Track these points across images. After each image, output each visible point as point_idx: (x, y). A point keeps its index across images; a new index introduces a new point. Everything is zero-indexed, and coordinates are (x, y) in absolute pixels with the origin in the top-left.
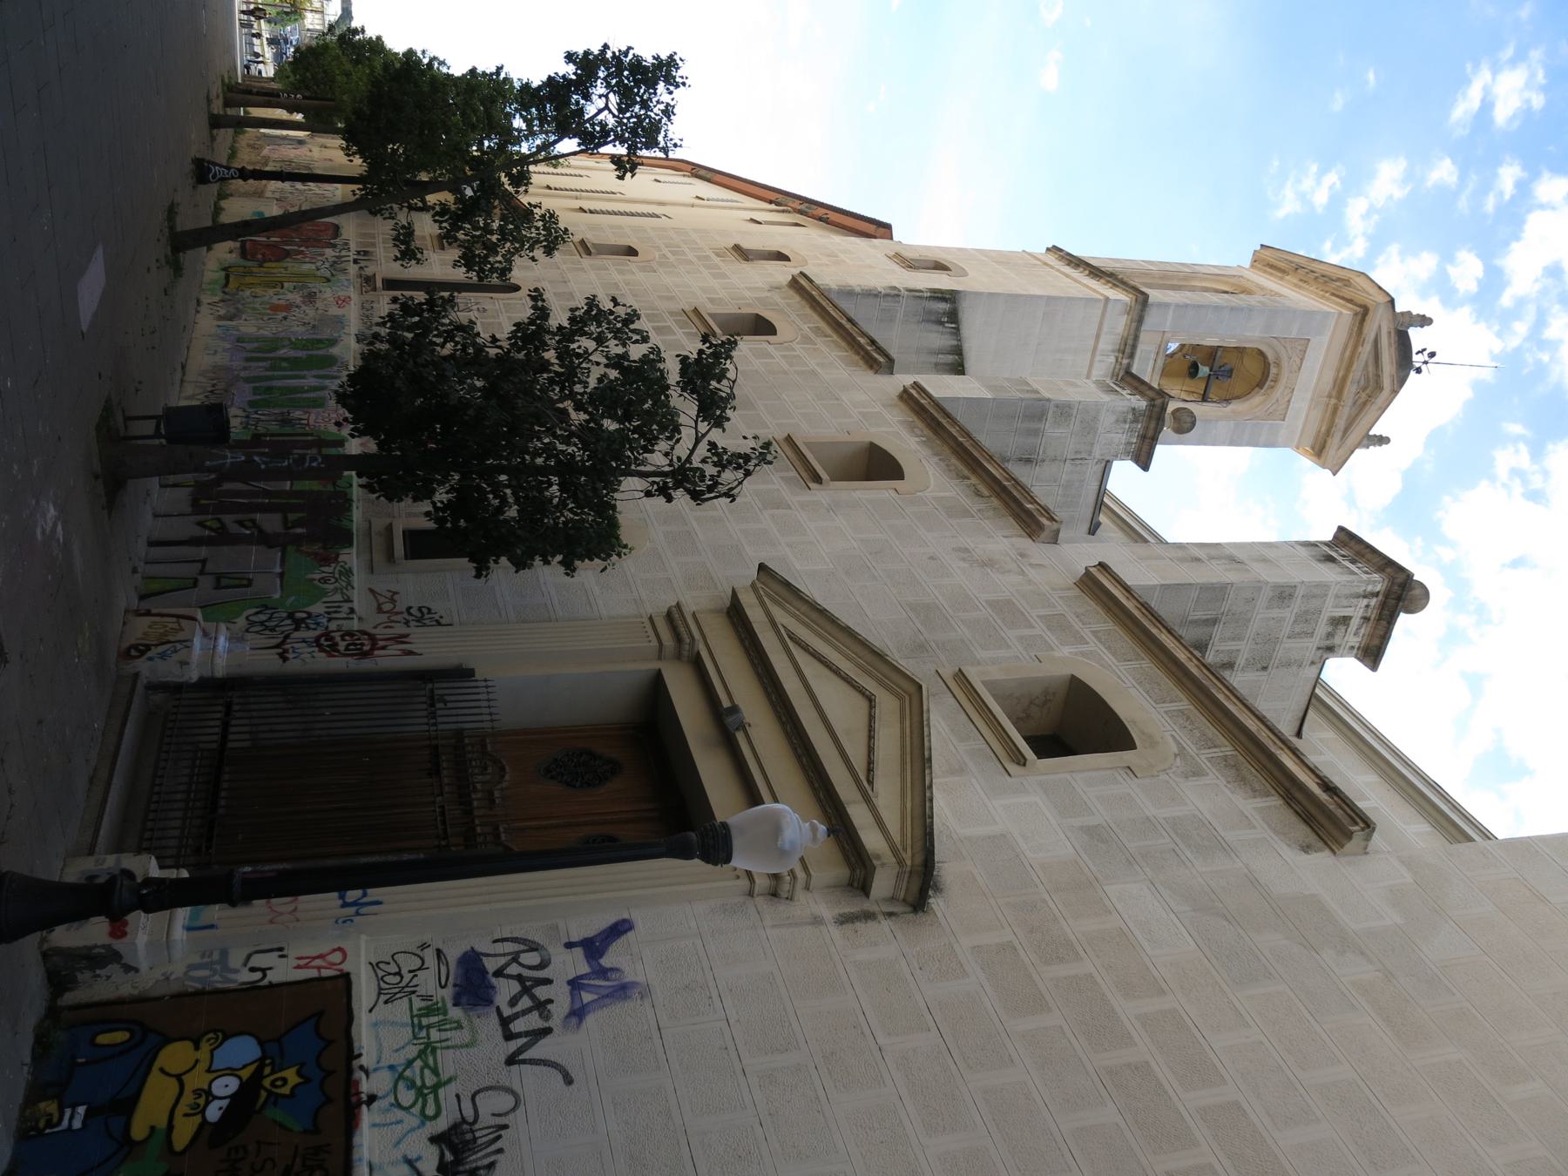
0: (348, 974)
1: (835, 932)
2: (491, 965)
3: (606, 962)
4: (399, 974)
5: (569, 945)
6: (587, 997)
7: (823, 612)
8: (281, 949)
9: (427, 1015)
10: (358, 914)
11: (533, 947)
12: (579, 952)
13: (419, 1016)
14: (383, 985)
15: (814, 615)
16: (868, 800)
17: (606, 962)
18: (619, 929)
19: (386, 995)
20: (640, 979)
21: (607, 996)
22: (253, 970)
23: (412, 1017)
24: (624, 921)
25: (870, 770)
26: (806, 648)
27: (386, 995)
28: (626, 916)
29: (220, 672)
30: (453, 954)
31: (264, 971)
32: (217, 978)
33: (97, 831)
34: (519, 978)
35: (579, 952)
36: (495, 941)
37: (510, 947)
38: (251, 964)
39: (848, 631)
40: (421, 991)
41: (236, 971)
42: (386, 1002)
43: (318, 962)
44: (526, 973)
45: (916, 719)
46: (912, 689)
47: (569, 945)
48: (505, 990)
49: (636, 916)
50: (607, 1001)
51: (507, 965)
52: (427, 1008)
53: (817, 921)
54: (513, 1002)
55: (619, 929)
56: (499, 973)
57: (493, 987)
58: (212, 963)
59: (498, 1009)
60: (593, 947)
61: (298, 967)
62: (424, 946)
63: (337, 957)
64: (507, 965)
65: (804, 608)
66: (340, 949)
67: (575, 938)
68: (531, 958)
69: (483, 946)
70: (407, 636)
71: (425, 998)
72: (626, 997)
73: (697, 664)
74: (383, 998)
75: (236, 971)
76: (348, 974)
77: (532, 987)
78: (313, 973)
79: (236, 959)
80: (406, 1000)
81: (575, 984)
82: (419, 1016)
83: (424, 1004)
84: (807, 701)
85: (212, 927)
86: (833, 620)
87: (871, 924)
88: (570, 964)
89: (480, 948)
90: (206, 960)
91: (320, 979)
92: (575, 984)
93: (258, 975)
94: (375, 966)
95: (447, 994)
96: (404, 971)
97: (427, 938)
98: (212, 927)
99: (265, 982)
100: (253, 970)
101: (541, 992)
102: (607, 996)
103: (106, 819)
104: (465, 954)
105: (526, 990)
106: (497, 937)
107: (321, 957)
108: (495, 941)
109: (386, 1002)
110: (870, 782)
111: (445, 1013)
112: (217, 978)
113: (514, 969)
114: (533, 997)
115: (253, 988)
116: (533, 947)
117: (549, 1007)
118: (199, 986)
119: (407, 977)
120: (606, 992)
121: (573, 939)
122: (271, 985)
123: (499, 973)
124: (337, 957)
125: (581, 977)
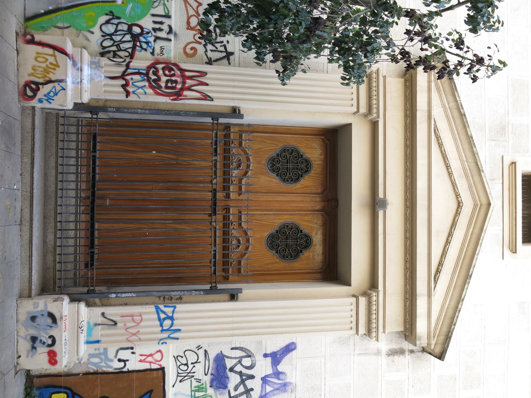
0: (164, 368)
1: (384, 360)
2: (229, 363)
3: (280, 368)
4: (186, 364)
5: (266, 355)
6: (269, 389)
7: (462, 116)
8: (132, 348)
9: (198, 391)
10: (169, 337)
11: (249, 356)
12: (269, 359)
13: (195, 391)
14: (180, 371)
15: (456, 114)
16: (429, 296)
17: (280, 368)
18: (289, 348)
19: (182, 377)
20: (293, 381)
21: (277, 389)
22: (120, 360)
23: (192, 391)
24: (293, 343)
25: (438, 271)
26: (440, 145)
27: (182, 377)
28: (294, 341)
29: (85, 99)
30: (212, 355)
31: (125, 361)
32: (103, 364)
33: (30, 269)
34: (240, 373)
35: (269, 359)
36: (232, 349)
37: (239, 353)
38: (118, 357)
39: (460, 300)
40: (196, 376)
41: (112, 361)
42: (180, 381)
43: (150, 359)
44: (245, 371)
45: (476, 231)
46: (484, 201)
47: (266, 355)
48: (234, 379)
49: (299, 340)
50: (276, 392)
51: (235, 365)
52: (198, 387)
53: (378, 353)
54: (236, 388)
55: (289, 348)
56: (231, 370)
57: (228, 378)
58: (100, 354)
59: (229, 390)
60: (276, 358)
61: (141, 361)
62: (199, 348)
63: (158, 356)
64: (235, 365)
65: (453, 104)
66: (160, 351)
67: (268, 352)
68: (247, 362)
69: (227, 352)
70: (203, 74)
71: (199, 381)
72: (285, 391)
73: (374, 125)
74: (179, 378)
75: (112, 361)
76: (164, 368)
77: (246, 380)
78: (146, 366)
79: (111, 354)
80: (189, 380)
81: (264, 380)
82: (195, 391)
83: (198, 384)
84: (425, 161)
85: (98, 342)
86: (465, 126)
87: (402, 357)
88: (263, 367)
89: (225, 353)
90: (97, 352)
91: (151, 370)
92: (264, 380)
93: (122, 364)
94: (176, 358)
95: (207, 379)
96: (189, 363)
97: (200, 342)
98: (98, 342)
99: (125, 370)
100: (120, 360)
101: (249, 383)
102: (277, 389)
103: (34, 264)
104: (218, 355)
105: (243, 382)
106: (233, 346)
107: (151, 355)
108: (232, 349)
109: (180, 381)
110: (436, 282)
111: (206, 392)
112: (103, 364)
113: (238, 368)
114: (245, 386)
115: (120, 373)
116: (249, 356)
117: (251, 392)
118: (95, 369)
119: (191, 366)
120: (276, 386)
121: (268, 352)
122: (129, 372)
123: (231, 370)
124: (158, 356)
125: (267, 376)
